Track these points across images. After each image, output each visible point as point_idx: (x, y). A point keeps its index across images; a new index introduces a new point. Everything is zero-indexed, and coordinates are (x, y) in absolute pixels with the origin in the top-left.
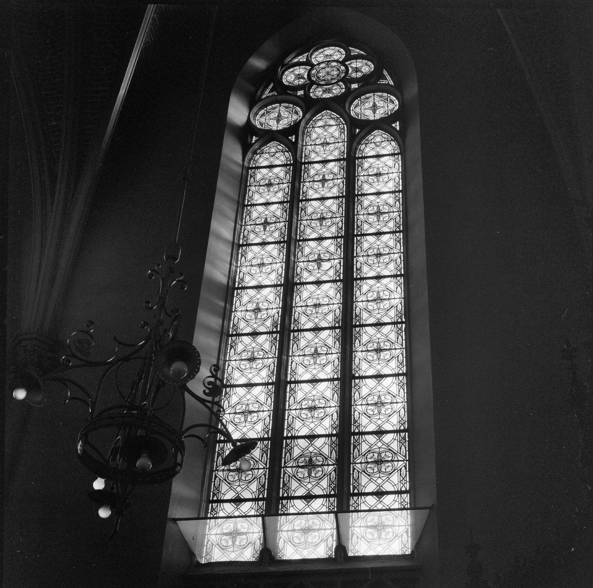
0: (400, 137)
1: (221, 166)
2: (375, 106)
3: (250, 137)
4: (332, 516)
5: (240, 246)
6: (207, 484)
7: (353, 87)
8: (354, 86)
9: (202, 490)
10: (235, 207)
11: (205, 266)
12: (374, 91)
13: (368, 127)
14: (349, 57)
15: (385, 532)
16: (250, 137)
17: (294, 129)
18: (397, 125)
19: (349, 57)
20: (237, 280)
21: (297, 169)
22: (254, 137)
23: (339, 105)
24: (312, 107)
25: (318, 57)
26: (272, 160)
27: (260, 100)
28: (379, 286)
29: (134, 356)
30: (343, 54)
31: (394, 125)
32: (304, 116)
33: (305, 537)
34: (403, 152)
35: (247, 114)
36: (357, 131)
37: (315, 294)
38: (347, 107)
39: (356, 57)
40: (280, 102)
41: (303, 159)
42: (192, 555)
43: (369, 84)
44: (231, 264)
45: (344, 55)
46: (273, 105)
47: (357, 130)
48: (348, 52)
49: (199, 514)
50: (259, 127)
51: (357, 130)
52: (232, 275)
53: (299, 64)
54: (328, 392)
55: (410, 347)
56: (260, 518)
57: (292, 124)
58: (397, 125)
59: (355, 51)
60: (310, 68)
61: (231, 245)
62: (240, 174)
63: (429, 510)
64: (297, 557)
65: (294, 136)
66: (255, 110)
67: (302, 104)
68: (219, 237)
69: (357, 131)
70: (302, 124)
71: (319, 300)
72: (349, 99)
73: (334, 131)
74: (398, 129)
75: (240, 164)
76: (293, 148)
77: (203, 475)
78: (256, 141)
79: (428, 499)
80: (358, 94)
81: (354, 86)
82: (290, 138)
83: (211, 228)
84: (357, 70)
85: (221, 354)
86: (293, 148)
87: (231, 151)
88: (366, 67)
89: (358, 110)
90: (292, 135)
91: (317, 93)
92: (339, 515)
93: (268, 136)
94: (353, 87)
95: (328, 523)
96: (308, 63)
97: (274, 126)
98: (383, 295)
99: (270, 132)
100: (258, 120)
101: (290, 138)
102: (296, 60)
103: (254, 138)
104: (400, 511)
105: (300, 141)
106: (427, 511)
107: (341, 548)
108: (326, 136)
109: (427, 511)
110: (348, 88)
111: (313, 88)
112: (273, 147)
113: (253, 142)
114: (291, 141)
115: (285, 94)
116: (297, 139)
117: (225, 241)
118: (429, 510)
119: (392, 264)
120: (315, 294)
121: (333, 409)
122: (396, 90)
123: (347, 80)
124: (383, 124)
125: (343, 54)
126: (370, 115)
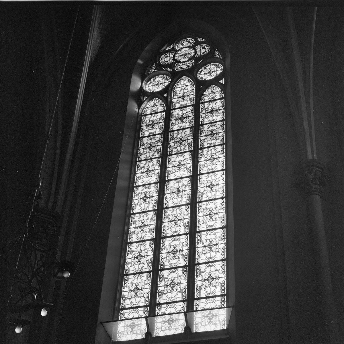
0: (223, 88)
2: (211, 71)
3: (141, 96)
13: (207, 84)
16: (141, 96)
18: (222, 81)
22: (145, 97)
24: (176, 77)
28: (211, 167)
29: (30, 268)
36: (201, 87)
42: (110, 338)
47: (201, 86)
48: (196, 40)
50: (148, 91)
51: (201, 86)
55: (228, 233)
56: (144, 319)
57: (99, 45)
59: (201, 40)
64: (164, 335)
67: (170, 75)
69: (201, 87)
78: (146, 99)
82: (166, 95)
89: (202, 76)
93: (152, 96)
96: (173, 50)
97: (157, 89)
103: (145, 98)
105: (169, 97)
119: (219, 192)
122: (222, 61)
124: (215, 81)
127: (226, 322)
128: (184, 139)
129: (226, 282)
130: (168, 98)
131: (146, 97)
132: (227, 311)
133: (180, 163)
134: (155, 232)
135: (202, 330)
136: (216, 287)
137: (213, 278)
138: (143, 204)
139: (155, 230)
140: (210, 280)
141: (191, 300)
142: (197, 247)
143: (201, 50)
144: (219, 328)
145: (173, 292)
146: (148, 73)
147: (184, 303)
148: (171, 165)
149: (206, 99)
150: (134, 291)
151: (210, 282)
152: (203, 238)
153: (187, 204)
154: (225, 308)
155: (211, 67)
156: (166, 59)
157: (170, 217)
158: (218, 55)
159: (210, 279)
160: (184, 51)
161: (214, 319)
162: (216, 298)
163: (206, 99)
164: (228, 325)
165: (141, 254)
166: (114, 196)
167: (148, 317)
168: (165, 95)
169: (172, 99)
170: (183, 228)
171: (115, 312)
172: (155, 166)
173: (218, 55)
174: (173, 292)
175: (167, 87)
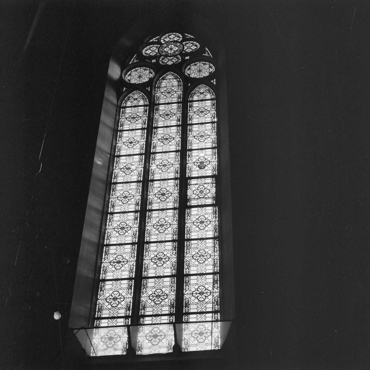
0: (215, 89)
1: (99, 133)
2: (200, 70)
4: (172, 327)
7: (186, 59)
8: (187, 58)
9: (89, 322)
10: (116, 109)
11: (100, 128)
12: (200, 61)
14: (185, 39)
15: (204, 335)
16: (123, 89)
19: (185, 39)
21: (152, 106)
23: (178, 69)
24: (161, 70)
25: (165, 39)
26: (134, 110)
27: (128, 65)
30: (181, 38)
31: (212, 81)
33: (155, 340)
36: (189, 86)
37: (162, 181)
39: (190, 39)
40: (140, 66)
43: (196, 57)
45: (182, 38)
46: (136, 69)
48: (184, 37)
49: (89, 326)
53: (153, 43)
54: (169, 249)
55: (219, 154)
58: (214, 82)
60: (159, 46)
66: (124, 72)
68: (105, 125)
70: (155, 80)
72: (184, 66)
73: (175, 83)
74: (215, 84)
77: (101, 225)
80: (189, 63)
81: (187, 58)
82: (148, 89)
83: (93, 173)
85: (107, 194)
87: (110, 96)
93: (134, 87)
94: (186, 59)
95: (169, 331)
96: (159, 43)
100: (127, 78)
101: (147, 88)
102: (151, 41)
106: (231, 322)
107: (177, 347)
108: (170, 87)
109: (231, 322)
110: (183, 59)
111: (161, 58)
112: (136, 95)
113: (124, 91)
114: (147, 90)
115: (144, 62)
119: (210, 140)
120: (162, 181)
123: (183, 54)
125: (181, 38)
130: (154, 80)
132: (222, 328)
135: (192, 349)
137: (204, 288)
138: (128, 169)
139: (145, 151)
143: (191, 47)
144: (164, 351)
145: (159, 290)
149: (195, 98)
150: (115, 293)
152: (193, 250)
156: (150, 51)
158: (208, 53)
160: (171, 44)
161: (204, 335)
166: (101, 115)
169: (148, 195)
170: (170, 234)
171: (91, 320)
172: (139, 136)
173: (208, 53)
175: (151, 80)
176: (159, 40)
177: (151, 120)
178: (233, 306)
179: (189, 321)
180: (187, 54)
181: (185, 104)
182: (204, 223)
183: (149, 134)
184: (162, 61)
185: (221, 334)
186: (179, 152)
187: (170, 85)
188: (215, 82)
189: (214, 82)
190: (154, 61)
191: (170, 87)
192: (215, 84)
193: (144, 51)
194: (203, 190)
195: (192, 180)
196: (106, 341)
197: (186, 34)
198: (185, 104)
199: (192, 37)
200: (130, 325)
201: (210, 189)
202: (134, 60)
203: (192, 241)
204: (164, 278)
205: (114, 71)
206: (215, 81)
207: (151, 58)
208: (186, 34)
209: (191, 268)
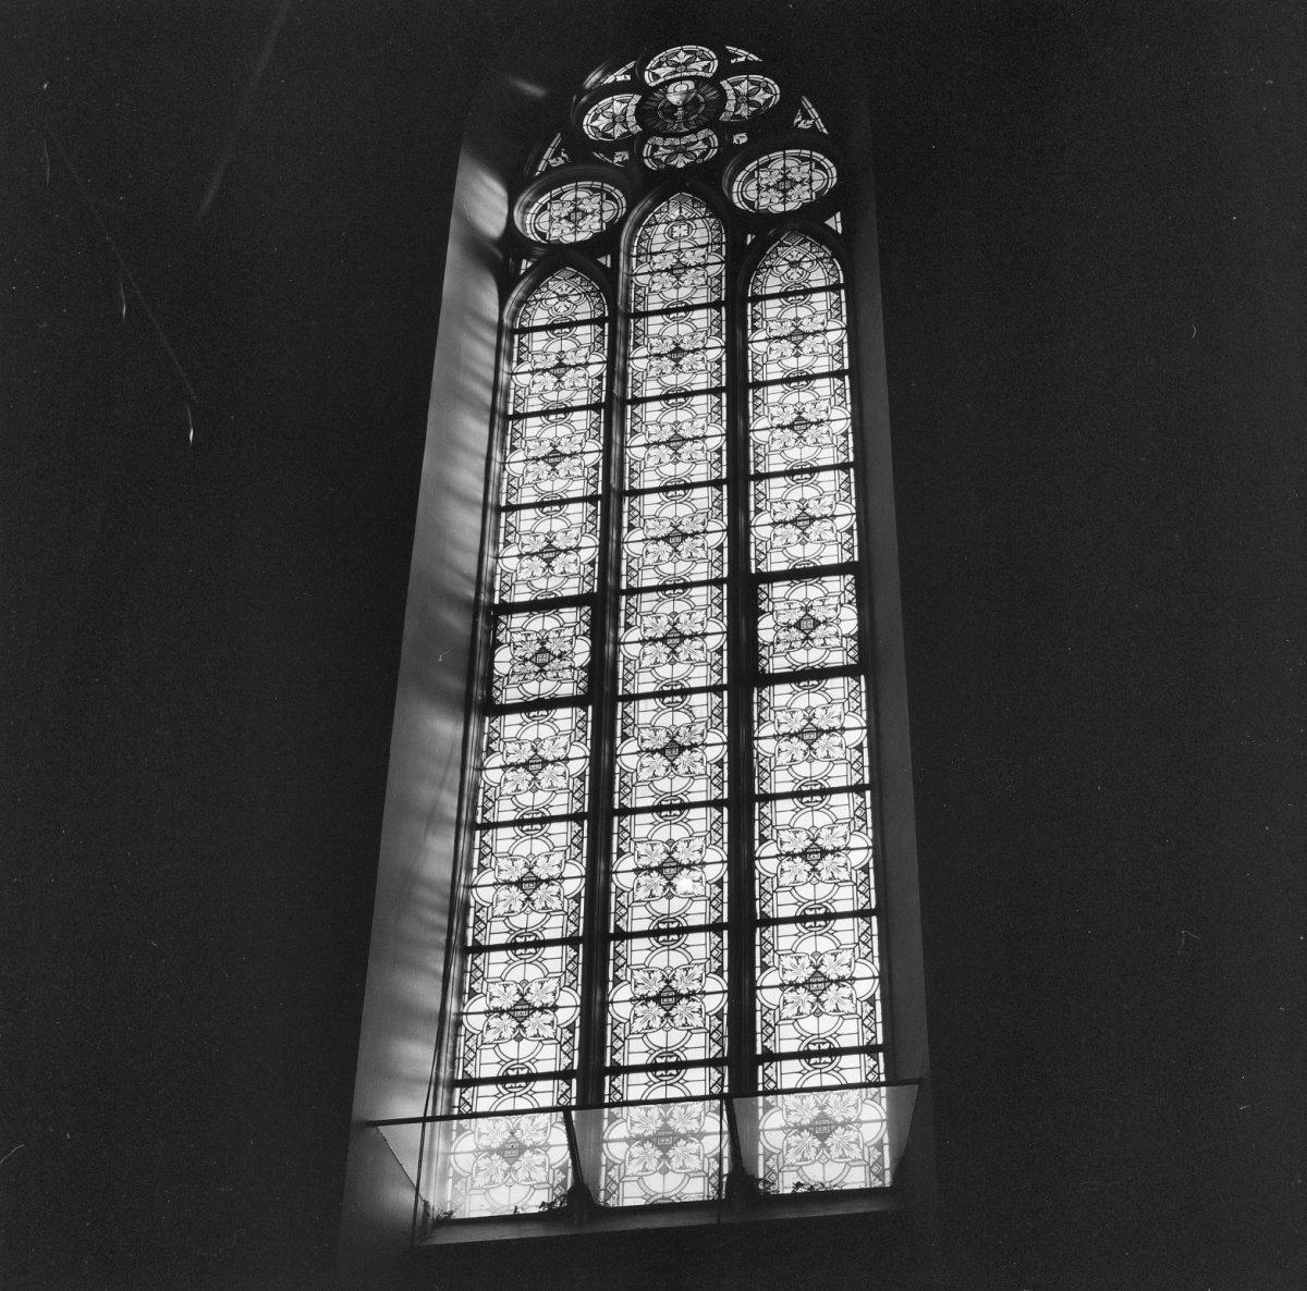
0: (841, 249)
2: (784, 182)
5: (499, 510)
6: (455, 989)
8: (741, 139)
14: (727, 69)
15: (835, 1134)
17: (608, 239)
20: (497, 587)
21: (619, 322)
23: (704, 185)
26: (557, 358)
28: (799, 454)
32: (630, 208)
33: (661, 1160)
34: (851, 288)
35: (506, 211)
36: (747, 244)
37: (663, 475)
38: (725, 181)
39: (747, 68)
41: (624, 579)
43: (771, 131)
44: (489, 459)
48: (724, 57)
52: (486, 577)
53: (617, 88)
58: (835, 223)
61: (487, 417)
62: (466, 643)
63: (917, 1086)
65: (609, 257)
66: (525, 197)
71: (673, 867)
72: (729, 170)
75: (485, 405)
76: (607, 284)
78: (528, 271)
79: (918, 1059)
81: (741, 139)
82: (598, 263)
84: (747, 99)
86: (607, 284)
88: (768, 93)
90: (604, 254)
91: (660, 152)
92: (736, 1101)
93: (554, 258)
95: (711, 1123)
97: (564, 234)
98: (827, 847)
99: (557, 247)
104: (864, 1090)
113: (522, 272)
115: (586, 161)
116: (615, 262)
117: (488, 323)
118: (917, 1086)
119: (832, 437)
121: (716, 748)
124: (806, 223)
126: (773, 203)
127: (890, 1150)
128: (688, 435)
129: (881, 995)
131: (529, 265)
133: (675, 528)
134: (583, 976)
136: (832, 765)
137: (831, 981)
138: (521, 874)
140: (815, 986)
141: (742, 1066)
142: (757, 855)
144: (857, 1179)
145: (666, 1004)
146: (530, 175)
147: (719, 1072)
148: (641, 440)
149: (773, 285)
150: (515, 1008)
151: (814, 863)
153: (710, 686)
154: (877, 1084)
155: (781, 162)
157: (652, 429)
158: (810, 119)
159: (818, 982)
161: (835, 1134)
162: (834, 796)
163: (773, 285)
164: (901, 1167)
165: (544, 564)
167: (574, 1108)
168: (606, 261)
170: (703, 461)
174: (666, 1004)
175: (614, 228)
176: (637, 75)
177: (616, 369)
178: (939, 1041)
179: (779, 1087)
180: (738, 125)
181: (736, 307)
182: (822, 736)
183: (614, 380)
184: (654, 74)
185: (890, 1129)
186: (722, 1065)
187: (680, 239)
188: (839, 226)
189: (835, 223)
190: (620, 157)
191: (678, 247)
192: (840, 231)
193: (587, 120)
194: (818, 620)
195: (775, 584)
196: (487, 1168)
197: (731, 49)
198: (736, 307)
199: (753, 57)
200: (574, 1108)
201: (837, 612)
202: (550, 159)
203: (780, 926)
204: (692, 488)
205: (485, 203)
206: (839, 219)
207: (611, 147)
208: (731, 49)
209: (786, 1178)
